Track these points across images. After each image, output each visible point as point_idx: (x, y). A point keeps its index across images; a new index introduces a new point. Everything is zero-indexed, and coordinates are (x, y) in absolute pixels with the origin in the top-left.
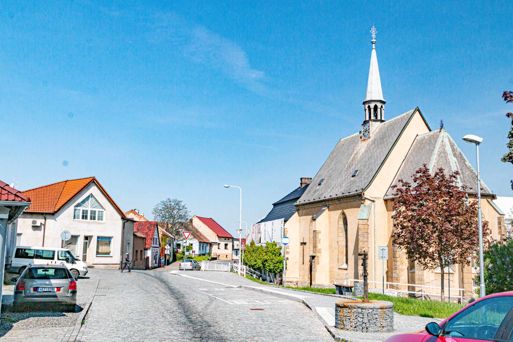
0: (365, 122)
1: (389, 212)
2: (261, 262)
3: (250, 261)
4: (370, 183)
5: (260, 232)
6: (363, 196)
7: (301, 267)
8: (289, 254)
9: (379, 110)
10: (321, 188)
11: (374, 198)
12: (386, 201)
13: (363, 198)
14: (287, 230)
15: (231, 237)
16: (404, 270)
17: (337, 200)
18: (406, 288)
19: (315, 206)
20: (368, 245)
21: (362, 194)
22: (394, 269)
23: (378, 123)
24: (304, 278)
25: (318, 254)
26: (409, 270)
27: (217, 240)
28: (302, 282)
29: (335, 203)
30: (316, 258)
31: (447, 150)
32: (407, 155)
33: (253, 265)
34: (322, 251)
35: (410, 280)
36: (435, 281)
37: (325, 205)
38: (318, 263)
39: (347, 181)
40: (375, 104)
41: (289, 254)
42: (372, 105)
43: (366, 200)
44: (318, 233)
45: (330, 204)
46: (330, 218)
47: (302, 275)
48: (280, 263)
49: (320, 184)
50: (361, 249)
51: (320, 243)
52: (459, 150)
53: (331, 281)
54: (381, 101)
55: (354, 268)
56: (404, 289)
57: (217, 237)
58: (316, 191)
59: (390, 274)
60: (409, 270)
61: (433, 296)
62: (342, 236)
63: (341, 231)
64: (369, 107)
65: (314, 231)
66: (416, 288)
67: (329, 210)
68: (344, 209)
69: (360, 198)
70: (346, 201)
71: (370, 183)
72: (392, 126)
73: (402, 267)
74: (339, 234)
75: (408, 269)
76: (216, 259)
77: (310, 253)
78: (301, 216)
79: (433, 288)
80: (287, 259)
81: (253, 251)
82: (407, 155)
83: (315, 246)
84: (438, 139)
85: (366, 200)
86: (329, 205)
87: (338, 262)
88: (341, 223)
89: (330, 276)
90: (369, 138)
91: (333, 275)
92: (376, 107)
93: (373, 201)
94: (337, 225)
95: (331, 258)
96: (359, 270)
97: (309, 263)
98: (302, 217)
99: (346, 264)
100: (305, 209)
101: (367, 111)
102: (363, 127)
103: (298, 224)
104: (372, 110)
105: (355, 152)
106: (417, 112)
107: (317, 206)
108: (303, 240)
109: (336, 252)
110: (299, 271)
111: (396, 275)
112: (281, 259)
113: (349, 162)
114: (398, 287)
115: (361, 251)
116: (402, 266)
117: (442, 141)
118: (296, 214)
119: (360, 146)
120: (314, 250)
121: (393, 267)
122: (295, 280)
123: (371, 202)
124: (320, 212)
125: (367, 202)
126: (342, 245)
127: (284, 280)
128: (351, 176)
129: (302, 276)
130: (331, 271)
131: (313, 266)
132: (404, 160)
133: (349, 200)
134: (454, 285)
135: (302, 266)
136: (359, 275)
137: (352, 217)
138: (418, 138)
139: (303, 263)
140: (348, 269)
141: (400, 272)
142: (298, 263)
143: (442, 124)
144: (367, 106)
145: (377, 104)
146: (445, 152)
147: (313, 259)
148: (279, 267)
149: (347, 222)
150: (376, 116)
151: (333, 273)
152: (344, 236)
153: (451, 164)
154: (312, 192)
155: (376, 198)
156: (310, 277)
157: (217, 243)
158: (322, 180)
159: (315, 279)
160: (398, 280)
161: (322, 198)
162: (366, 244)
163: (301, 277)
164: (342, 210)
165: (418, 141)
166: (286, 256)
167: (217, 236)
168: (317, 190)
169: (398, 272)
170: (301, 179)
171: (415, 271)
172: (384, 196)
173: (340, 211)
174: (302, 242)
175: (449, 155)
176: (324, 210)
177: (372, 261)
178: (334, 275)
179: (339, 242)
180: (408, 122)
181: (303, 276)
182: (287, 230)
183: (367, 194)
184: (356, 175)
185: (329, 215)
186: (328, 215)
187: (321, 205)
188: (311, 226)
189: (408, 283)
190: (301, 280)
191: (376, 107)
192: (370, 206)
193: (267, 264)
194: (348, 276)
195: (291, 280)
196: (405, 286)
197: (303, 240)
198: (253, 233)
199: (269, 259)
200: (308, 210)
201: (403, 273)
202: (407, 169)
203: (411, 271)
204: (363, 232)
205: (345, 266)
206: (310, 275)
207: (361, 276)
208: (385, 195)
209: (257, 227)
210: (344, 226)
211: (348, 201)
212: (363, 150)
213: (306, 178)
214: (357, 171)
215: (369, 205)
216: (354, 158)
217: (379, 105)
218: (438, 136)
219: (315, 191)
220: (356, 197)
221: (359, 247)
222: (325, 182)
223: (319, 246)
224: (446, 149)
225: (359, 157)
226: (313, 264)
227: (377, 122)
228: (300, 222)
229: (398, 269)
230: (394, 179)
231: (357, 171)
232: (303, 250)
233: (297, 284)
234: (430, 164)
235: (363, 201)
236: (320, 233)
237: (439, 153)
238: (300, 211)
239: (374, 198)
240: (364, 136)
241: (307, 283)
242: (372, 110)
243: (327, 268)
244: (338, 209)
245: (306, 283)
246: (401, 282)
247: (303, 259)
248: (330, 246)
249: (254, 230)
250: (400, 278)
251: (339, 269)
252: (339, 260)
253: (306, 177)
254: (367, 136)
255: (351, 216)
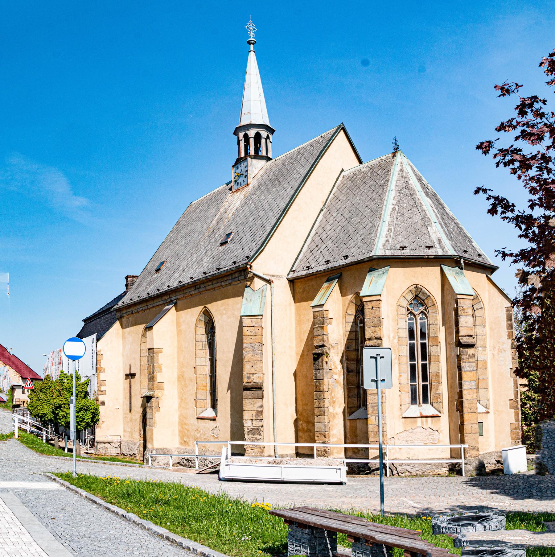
0: (239, 161)
1: (298, 304)
2: (52, 410)
3: (36, 408)
4: (262, 246)
5: (62, 363)
6: (249, 270)
7: (126, 417)
8: (106, 394)
9: (263, 141)
10: (160, 275)
11: (271, 276)
12: (292, 282)
13: (250, 275)
14: (102, 352)
15: (39, 378)
16: (336, 416)
17: (193, 289)
18: (341, 451)
19: (151, 306)
20: (262, 367)
21: (248, 266)
22: (318, 414)
23: (263, 162)
24: (131, 436)
25: (157, 393)
26: (347, 415)
27: (21, 383)
28: (128, 443)
29: (188, 294)
30: (154, 400)
31: (413, 185)
32: (326, 202)
33: (40, 415)
34: (165, 386)
35: (348, 435)
36: (405, 433)
37: (169, 300)
38: (158, 409)
39: (210, 254)
40: (256, 132)
41: (106, 394)
42: (252, 133)
43: (256, 279)
44: (158, 353)
45: (178, 297)
46: (178, 324)
47: (129, 430)
48: (86, 410)
49: (158, 270)
50: (249, 378)
51: (160, 371)
52: (430, 187)
53: (183, 442)
54: (266, 127)
55: (229, 416)
56: (338, 453)
57: (21, 378)
58: (151, 281)
59: (301, 425)
60: (347, 415)
61: (401, 465)
62: (204, 355)
63: (200, 347)
64: (246, 137)
65: (149, 349)
66: (370, 451)
67: (177, 310)
68: (207, 304)
69: (243, 277)
70: (211, 287)
71: (262, 246)
72: (294, 160)
73: (334, 410)
74: (197, 352)
75: (344, 413)
76: (18, 406)
77: (142, 393)
78: (126, 328)
79: (400, 449)
80: (103, 403)
81: (41, 390)
82: (326, 202)
83: (151, 378)
84: (393, 167)
85: (256, 279)
86: (177, 299)
87: (196, 406)
88: (202, 331)
89: (180, 432)
90: (248, 185)
91: (186, 431)
92: (258, 137)
93: (269, 282)
94: (192, 335)
95: (182, 399)
96: (246, 420)
97: (141, 410)
98: (128, 329)
99: (211, 409)
100: (132, 313)
101: (242, 144)
102: (236, 170)
103: (121, 342)
104: (252, 141)
105: (222, 210)
106: (342, 133)
107: (154, 305)
108: (130, 369)
109: (192, 388)
110: (124, 424)
111: (323, 428)
112: (87, 403)
113: (211, 226)
114: (327, 450)
115: (249, 381)
116: (334, 407)
117: (402, 171)
118: (117, 325)
119: (229, 201)
120: (150, 386)
121: (316, 411)
122: (116, 439)
123: (264, 283)
124: (160, 314)
125: (258, 283)
126: (204, 373)
127: (97, 439)
128: (219, 244)
129: (129, 432)
130: (182, 423)
131: (148, 416)
132: (322, 210)
133: (219, 285)
134: (441, 438)
135: (129, 415)
136: (246, 430)
137: (224, 316)
138: (343, 174)
139: (130, 410)
140: (217, 418)
141: (331, 419)
142: (121, 411)
143: (396, 144)
144: (241, 135)
145: (259, 131)
146: (408, 188)
147: (148, 402)
148: (84, 419)
149: (213, 327)
150: (257, 149)
151: (186, 427)
152: (208, 356)
153: (425, 208)
154: (145, 285)
155: (273, 276)
156: (142, 434)
157: (21, 386)
158: (162, 263)
159: (152, 440)
160: (326, 436)
161: (164, 288)
162: (258, 366)
163: (127, 435)
164: (203, 306)
165: (345, 178)
166: (101, 398)
167: (21, 377)
168: (154, 280)
169: (327, 421)
170: (127, 278)
171: (369, 416)
172: (289, 274)
173: (200, 308)
174: (128, 373)
175: (417, 192)
176: (168, 310)
177: (268, 401)
178: (188, 430)
179: (198, 368)
180: (327, 144)
181: (131, 433)
182: (102, 352)
183: (257, 267)
184: (229, 240)
185: (178, 318)
186: (175, 318)
187: (161, 302)
188: (143, 344)
189: (345, 443)
190: (127, 439)
191: (258, 137)
192: (263, 290)
193: (61, 414)
194: (217, 432)
195: (109, 439)
196: (340, 447)
197: (130, 369)
198: (53, 365)
199: (64, 404)
200: (138, 315)
201: (336, 421)
202: (332, 222)
203: (351, 417)
204: (251, 341)
205: (210, 413)
206: (142, 430)
207: (248, 432)
208: (291, 271)
209: (57, 355)
210: (208, 337)
211: (215, 286)
212: (238, 204)
213: (133, 276)
214: (228, 235)
215: (261, 289)
216: (221, 219)
217: (264, 133)
218: (391, 164)
219: (151, 282)
220: (233, 276)
221: (244, 373)
222: (167, 264)
223: (159, 377)
224: (410, 182)
225: (230, 215)
226: (148, 410)
227: (260, 161)
228: (124, 337)
229: (326, 414)
230: (305, 242)
231: (228, 235)
232: (130, 387)
233: (120, 446)
234: (384, 207)
235: (247, 281)
236: (161, 352)
237: (399, 188)
238: (124, 320)
239: (271, 276)
240: (238, 185)
241: (138, 444)
242: (252, 141)
243: (175, 419)
244: (196, 306)
245: (135, 444)
246: (332, 440)
247: (130, 404)
248: (181, 377)
249: (54, 359)
250: (331, 433)
251: (198, 418)
252: (198, 401)
253: (135, 275)
254: (243, 184)
255: (222, 314)
